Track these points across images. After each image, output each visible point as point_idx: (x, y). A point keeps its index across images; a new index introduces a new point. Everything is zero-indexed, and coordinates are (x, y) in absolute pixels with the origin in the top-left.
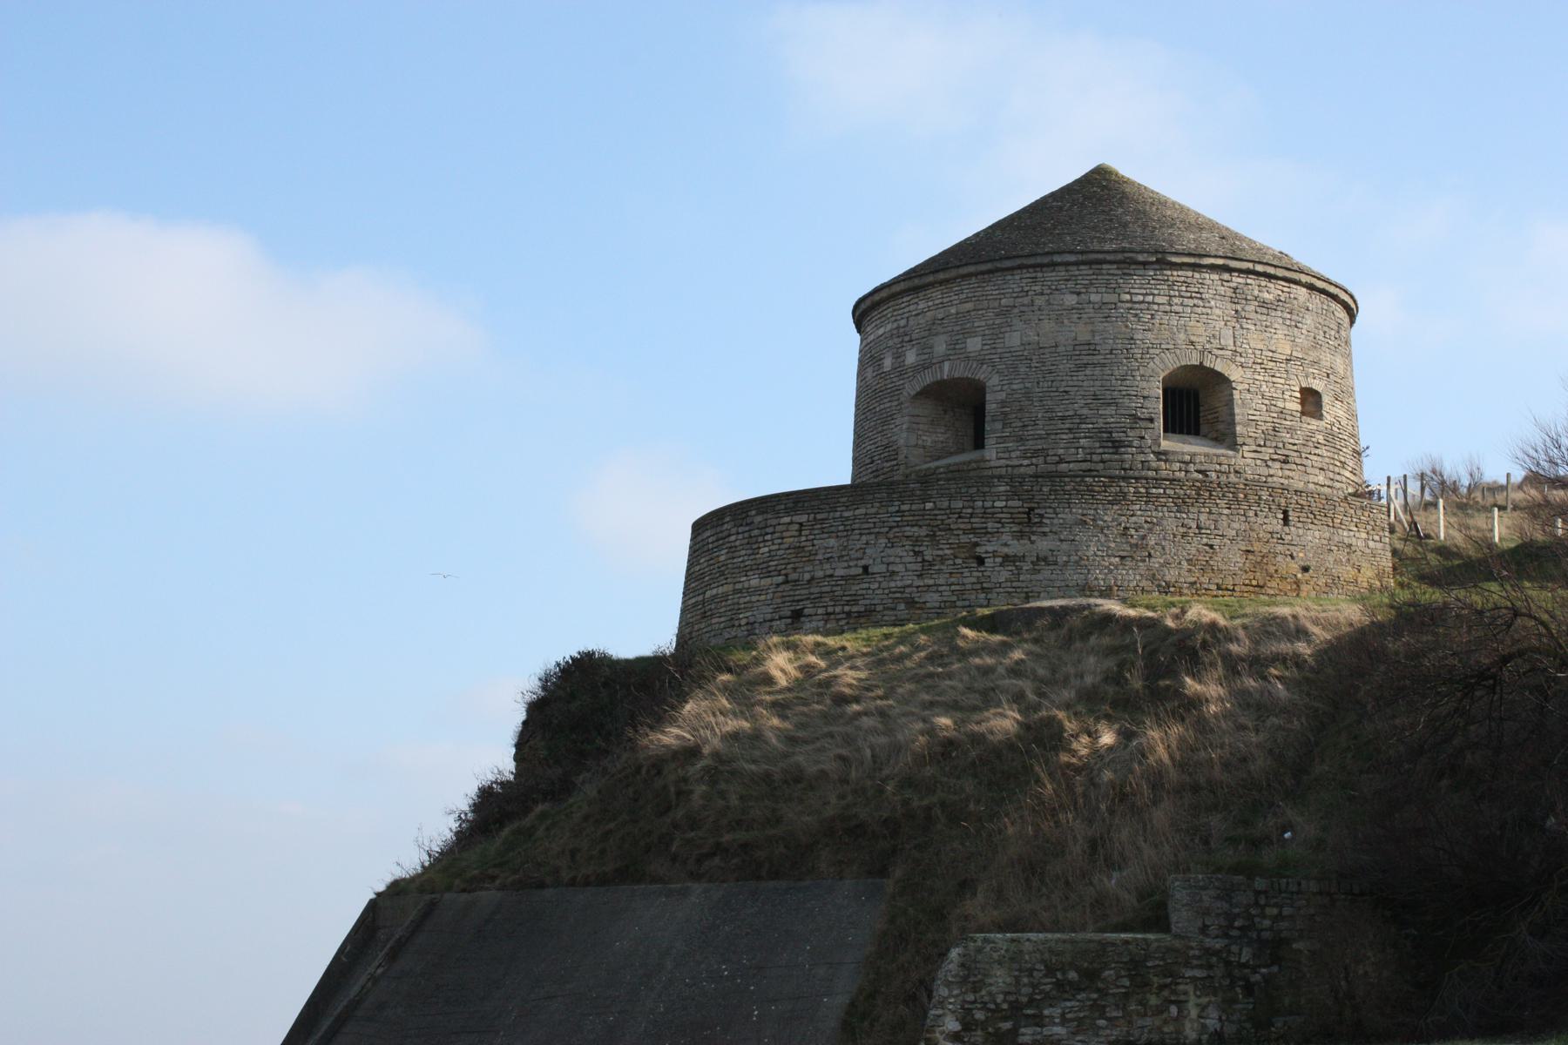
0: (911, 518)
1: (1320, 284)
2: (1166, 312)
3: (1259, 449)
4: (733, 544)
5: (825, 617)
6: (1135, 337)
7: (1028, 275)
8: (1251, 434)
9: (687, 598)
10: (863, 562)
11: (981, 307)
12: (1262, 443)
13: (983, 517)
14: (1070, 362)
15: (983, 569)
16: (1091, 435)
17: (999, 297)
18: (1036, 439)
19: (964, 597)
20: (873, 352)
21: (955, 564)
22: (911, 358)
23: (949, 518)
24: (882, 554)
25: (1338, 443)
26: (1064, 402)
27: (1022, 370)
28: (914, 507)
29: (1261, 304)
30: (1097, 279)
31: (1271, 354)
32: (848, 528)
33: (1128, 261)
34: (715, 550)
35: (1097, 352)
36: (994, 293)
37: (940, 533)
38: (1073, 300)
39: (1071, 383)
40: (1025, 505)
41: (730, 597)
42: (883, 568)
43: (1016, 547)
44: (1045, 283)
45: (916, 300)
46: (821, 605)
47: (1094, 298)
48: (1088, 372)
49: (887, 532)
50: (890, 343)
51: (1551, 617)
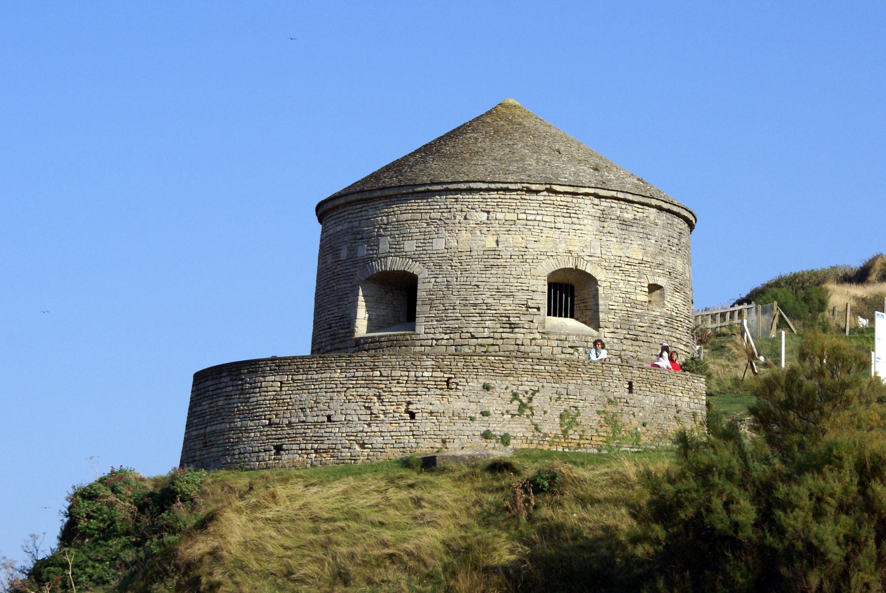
0: (363, 382)
1: (666, 206)
2: (552, 228)
3: (616, 331)
4: (229, 394)
6: (529, 246)
8: (610, 320)
9: (191, 429)
10: (328, 413)
11: (415, 218)
12: (619, 326)
13: (415, 384)
14: (480, 263)
15: (414, 421)
16: (494, 318)
19: (400, 441)
20: (332, 243)
25: (675, 324)
26: (475, 293)
29: (621, 222)
30: (502, 202)
31: (627, 260)
32: (317, 386)
33: (525, 189)
34: (215, 396)
35: (501, 257)
39: (480, 279)
40: (445, 376)
41: (226, 433)
45: (367, 208)
47: (500, 216)
48: (493, 272)
50: (346, 239)
51: (418, 561)
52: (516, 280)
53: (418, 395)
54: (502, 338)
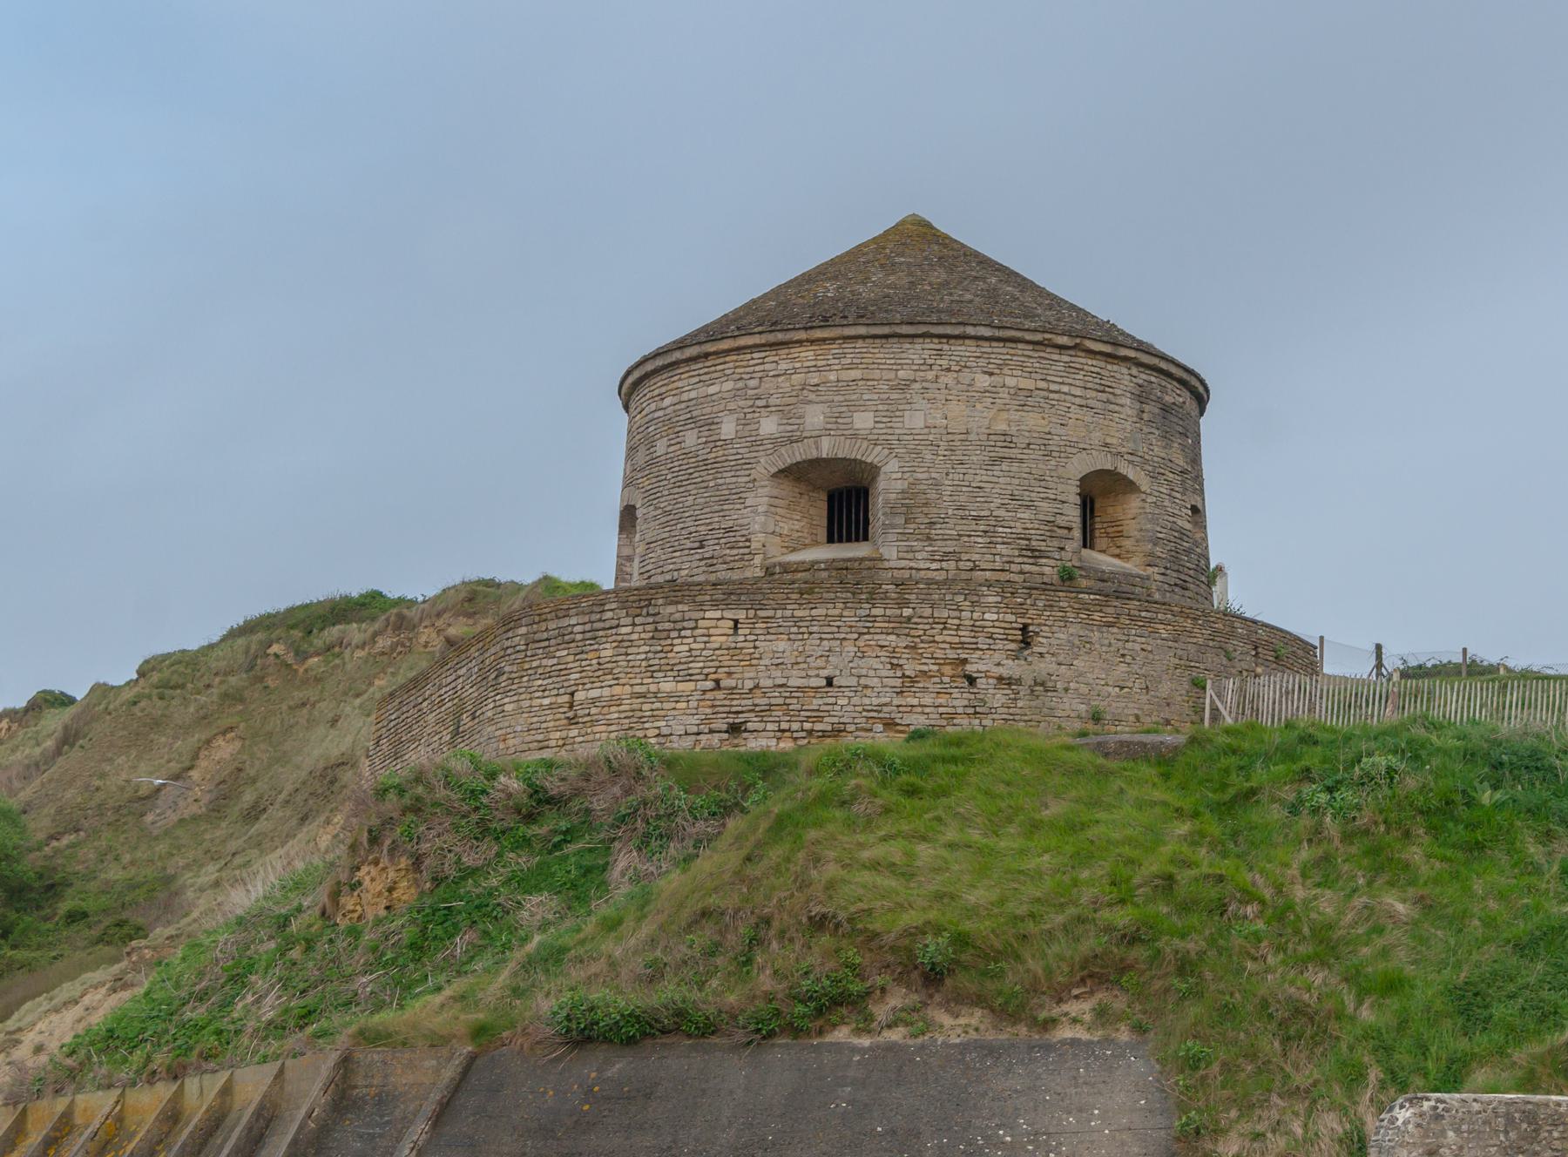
0: (886, 625)
4: (626, 637)
5: (779, 734)
7: (932, 346)
10: (825, 673)
11: (872, 377)
17: (895, 367)
18: (946, 540)
21: (942, 682)
22: (769, 426)
23: (933, 628)
24: (851, 665)
27: (927, 457)
28: (888, 612)
32: (804, 630)
35: (1014, 445)
36: (888, 362)
37: (922, 645)
38: (985, 381)
40: (1019, 620)
42: (853, 681)
43: (1011, 668)
44: (952, 358)
45: (776, 358)
46: (771, 719)
47: (1010, 382)
48: (1004, 467)
49: (856, 640)
52: (1038, 484)
53: (978, 649)
54: (1021, 572)
